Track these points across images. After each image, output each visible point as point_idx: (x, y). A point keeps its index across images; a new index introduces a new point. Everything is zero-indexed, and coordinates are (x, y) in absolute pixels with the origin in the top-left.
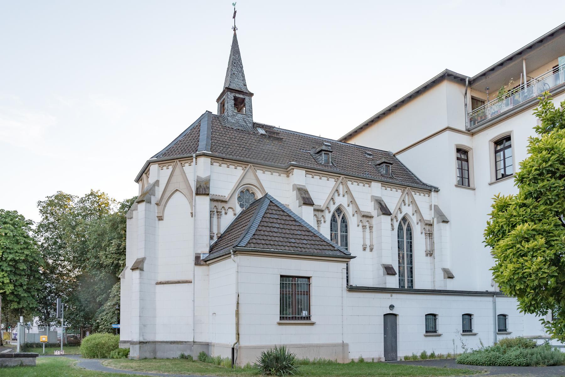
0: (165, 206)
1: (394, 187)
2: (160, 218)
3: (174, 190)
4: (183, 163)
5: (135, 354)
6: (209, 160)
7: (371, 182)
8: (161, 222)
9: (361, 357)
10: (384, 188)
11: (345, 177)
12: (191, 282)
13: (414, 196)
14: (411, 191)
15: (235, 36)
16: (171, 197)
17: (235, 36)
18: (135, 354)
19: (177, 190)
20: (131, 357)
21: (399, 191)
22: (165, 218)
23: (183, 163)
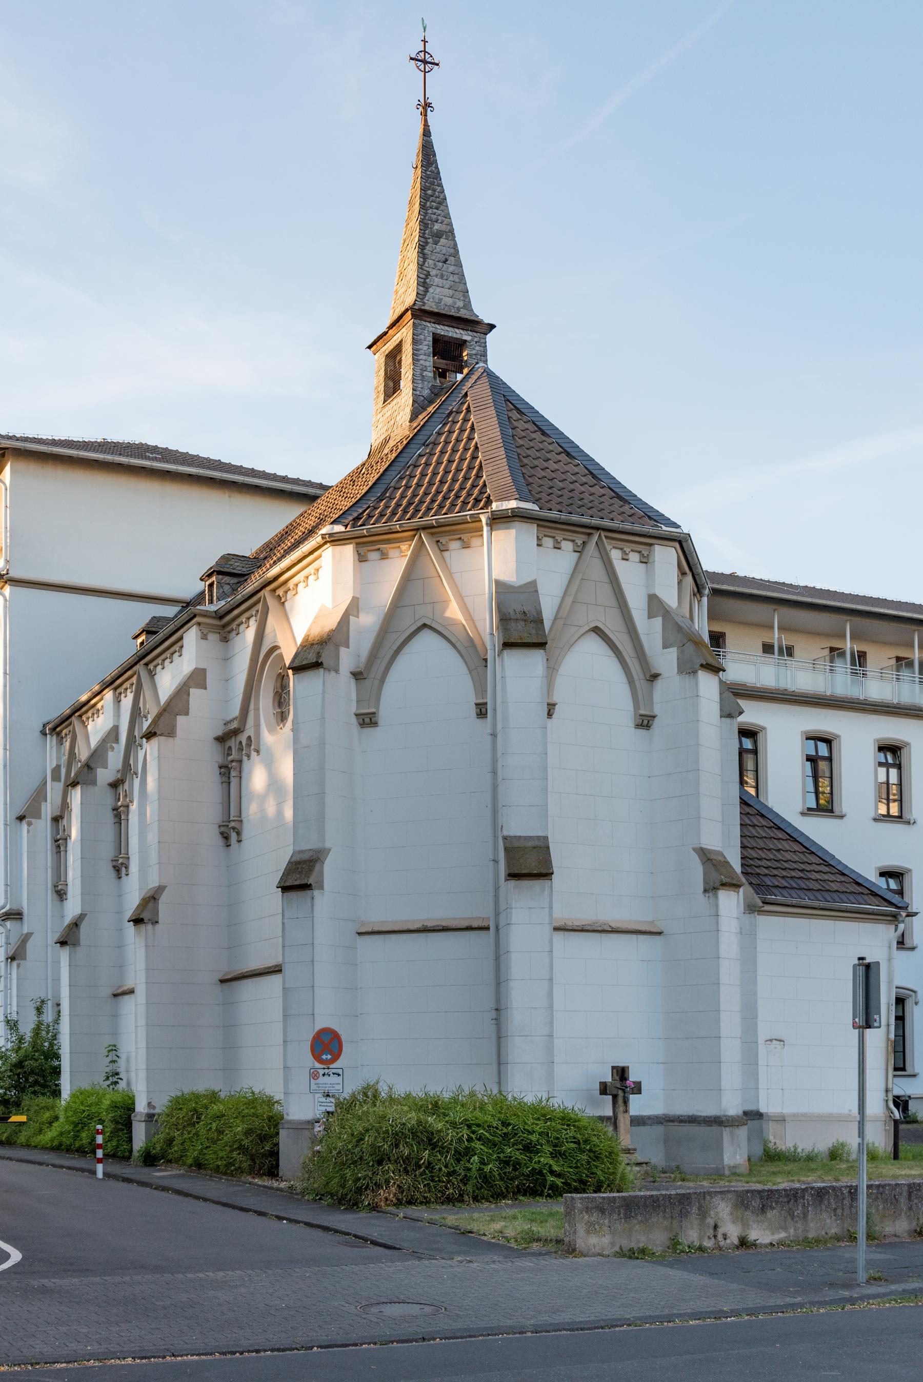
0: (383, 681)
1: (635, 547)
2: (367, 720)
3: (414, 628)
4: (443, 540)
5: (738, 1157)
6: (531, 530)
7: (651, 545)
8: (369, 731)
9: (915, 1114)
10: (548, 542)
11: (606, 537)
12: (487, 928)
13: (620, 566)
14: (608, 547)
15: (427, 133)
16: (402, 652)
17: (427, 133)
18: (738, 1157)
19: (425, 626)
20: (730, 1167)
21: (567, 546)
22: (384, 715)
23: (443, 540)
